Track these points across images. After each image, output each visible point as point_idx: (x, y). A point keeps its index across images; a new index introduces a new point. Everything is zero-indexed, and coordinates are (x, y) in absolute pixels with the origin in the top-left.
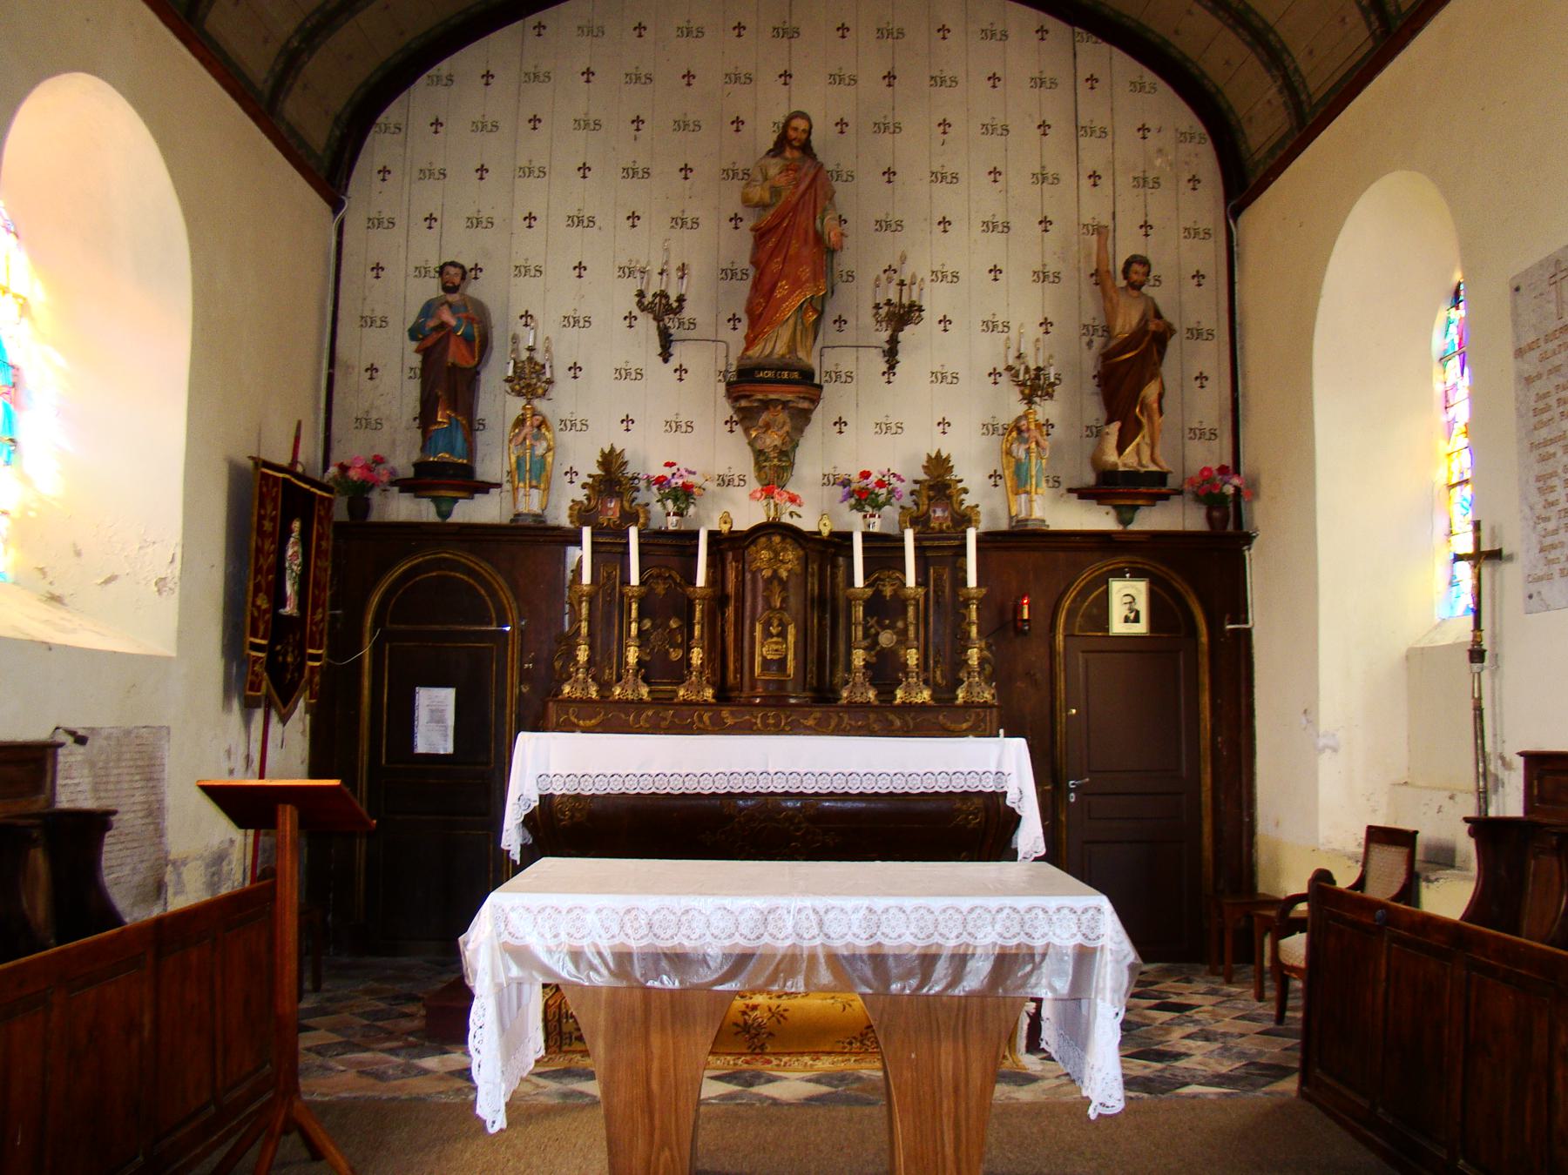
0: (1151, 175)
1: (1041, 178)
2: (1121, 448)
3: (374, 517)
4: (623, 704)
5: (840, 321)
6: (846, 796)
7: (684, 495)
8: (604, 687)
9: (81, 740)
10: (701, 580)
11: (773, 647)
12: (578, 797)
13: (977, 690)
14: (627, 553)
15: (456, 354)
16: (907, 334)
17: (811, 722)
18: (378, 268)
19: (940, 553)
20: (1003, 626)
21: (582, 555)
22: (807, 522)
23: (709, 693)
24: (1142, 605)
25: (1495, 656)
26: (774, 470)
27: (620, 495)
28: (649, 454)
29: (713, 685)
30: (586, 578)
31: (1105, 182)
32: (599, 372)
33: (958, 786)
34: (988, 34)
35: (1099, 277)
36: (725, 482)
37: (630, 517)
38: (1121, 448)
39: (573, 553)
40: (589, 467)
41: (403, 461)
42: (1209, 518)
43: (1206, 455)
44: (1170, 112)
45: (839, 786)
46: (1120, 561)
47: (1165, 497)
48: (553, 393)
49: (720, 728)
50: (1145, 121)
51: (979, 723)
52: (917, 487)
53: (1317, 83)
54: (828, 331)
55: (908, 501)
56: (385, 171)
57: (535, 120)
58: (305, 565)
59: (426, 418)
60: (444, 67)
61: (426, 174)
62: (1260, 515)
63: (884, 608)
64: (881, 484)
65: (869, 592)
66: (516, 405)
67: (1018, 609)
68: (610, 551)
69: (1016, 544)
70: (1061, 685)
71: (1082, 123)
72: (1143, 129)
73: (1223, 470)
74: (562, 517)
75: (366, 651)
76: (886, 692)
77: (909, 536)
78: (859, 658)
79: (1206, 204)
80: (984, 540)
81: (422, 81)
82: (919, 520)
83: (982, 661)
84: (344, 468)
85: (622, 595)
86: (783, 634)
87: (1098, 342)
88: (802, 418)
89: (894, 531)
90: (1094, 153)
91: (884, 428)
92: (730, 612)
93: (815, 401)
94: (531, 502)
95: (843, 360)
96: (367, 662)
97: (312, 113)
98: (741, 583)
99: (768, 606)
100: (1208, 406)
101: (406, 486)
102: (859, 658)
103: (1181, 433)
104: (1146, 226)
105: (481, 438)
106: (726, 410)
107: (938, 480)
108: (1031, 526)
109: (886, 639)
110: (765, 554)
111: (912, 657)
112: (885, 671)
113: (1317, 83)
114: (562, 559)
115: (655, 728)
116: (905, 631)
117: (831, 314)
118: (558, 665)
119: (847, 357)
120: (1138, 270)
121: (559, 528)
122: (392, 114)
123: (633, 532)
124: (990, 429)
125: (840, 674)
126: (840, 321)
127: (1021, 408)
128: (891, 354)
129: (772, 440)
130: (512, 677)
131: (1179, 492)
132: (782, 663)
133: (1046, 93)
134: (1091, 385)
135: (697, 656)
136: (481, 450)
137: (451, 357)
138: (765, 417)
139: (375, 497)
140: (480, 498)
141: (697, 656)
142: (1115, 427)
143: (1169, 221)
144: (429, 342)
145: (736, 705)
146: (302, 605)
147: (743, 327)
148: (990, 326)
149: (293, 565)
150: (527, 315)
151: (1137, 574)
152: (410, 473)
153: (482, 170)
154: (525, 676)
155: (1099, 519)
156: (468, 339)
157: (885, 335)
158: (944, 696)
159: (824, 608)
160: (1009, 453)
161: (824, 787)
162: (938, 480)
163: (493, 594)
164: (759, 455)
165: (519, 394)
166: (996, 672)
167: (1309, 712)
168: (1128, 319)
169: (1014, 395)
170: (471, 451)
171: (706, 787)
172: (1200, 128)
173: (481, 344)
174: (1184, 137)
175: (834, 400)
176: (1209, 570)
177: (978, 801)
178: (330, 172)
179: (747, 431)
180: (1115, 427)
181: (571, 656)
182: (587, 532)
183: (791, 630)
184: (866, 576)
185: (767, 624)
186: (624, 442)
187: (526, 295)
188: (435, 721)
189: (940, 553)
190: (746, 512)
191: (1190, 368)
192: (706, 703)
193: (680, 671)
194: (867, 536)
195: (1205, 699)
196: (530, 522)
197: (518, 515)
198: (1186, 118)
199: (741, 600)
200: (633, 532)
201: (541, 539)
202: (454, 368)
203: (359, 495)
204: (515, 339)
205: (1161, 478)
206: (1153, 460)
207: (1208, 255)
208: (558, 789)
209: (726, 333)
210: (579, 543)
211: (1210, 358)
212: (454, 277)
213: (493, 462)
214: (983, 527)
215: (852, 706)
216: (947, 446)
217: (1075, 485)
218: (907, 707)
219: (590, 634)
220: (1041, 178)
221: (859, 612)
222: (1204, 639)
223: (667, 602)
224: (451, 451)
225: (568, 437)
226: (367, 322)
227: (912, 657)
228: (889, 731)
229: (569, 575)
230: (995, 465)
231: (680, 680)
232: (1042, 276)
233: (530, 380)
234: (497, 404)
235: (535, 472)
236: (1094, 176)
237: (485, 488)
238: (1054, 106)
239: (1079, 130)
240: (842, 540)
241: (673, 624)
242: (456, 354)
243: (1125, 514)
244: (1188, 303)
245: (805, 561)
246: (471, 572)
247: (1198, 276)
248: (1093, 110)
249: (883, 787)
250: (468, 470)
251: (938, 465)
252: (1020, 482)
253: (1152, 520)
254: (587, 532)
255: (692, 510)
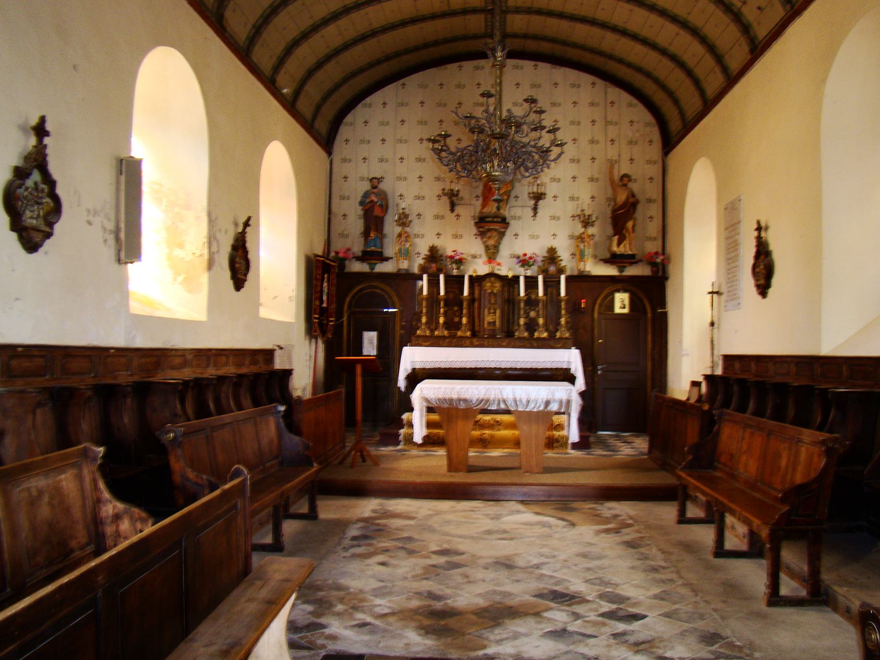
0: (634, 140)
1: (592, 142)
2: (619, 244)
3: (347, 270)
4: (438, 337)
5: (516, 197)
6: (516, 369)
7: (460, 262)
8: (432, 331)
9: (281, 348)
10: (466, 293)
11: (491, 317)
12: (424, 369)
13: (563, 333)
14: (439, 283)
15: (377, 212)
16: (541, 202)
17: (504, 344)
18: (346, 177)
19: (552, 283)
20: (574, 309)
21: (424, 283)
22: (503, 271)
23: (468, 334)
24: (627, 302)
25: (719, 325)
26: (492, 253)
27: (436, 262)
28: (449, 247)
29: (470, 330)
30: (425, 292)
31: (616, 143)
32: (428, 215)
33: (554, 366)
34: (573, 86)
35: (612, 182)
36: (474, 257)
37: (440, 271)
38: (619, 244)
39: (420, 283)
40: (424, 251)
41: (357, 248)
42: (652, 271)
43: (652, 247)
44: (641, 114)
45: (513, 366)
46: (619, 286)
47: (636, 263)
48: (411, 225)
49: (472, 345)
50: (633, 117)
51: (564, 344)
52: (435, 417)
53: (761, 32)
54: (512, 201)
55: (540, 264)
56: (347, 140)
57: (403, 121)
58: (328, 289)
59: (366, 234)
60: (368, 100)
61: (362, 142)
62: (672, 269)
63: (531, 302)
64: (531, 258)
65: (525, 298)
66: (398, 229)
67: (580, 304)
68: (434, 283)
69: (578, 280)
70: (596, 331)
71: (609, 119)
72: (631, 122)
73: (656, 253)
74: (416, 270)
75: (345, 318)
76: (531, 334)
77: (540, 279)
78: (522, 321)
79: (655, 151)
80: (569, 279)
81: (360, 105)
82: (544, 271)
83: (567, 322)
84: (337, 253)
85: (437, 298)
86: (495, 313)
87: (612, 204)
88: (502, 234)
89: (535, 274)
90: (612, 132)
91: (533, 237)
92: (476, 304)
93: (506, 228)
94: (404, 265)
95: (517, 211)
96: (345, 323)
97: (322, 125)
98: (480, 294)
99: (490, 303)
100: (653, 228)
101: (358, 259)
102: (522, 321)
103: (642, 238)
104: (631, 160)
105: (386, 241)
106: (474, 230)
107: (552, 256)
108: (586, 274)
109: (532, 314)
110: (489, 284)
111: (541, 321)
112: (531, 326)
113: (690, 113)
114: (415, 285)
115: (450, 345)
116: (538, 311)
117: (513, 194)
118: (414, 323)
119: (518, 211)
120: (626, 178)
121: (413, 274)
122: (349, 118)
123: (442, 277)
124: (572, 237)
125: (516, 327)
126: (516, 197)
127: (583, 230)
128: (535, 209)
129: (491, 242)
130: (398, 327)
131: (641, 261)
132: (494, 323)
133: (594, 108)
134: (609, 221)
135: (464, 320)
136: (385, 247)
137: (374, 211)
138: (489, 234)
139: (347, 262)
140: (385, 263)
141: (464, 320)
142: (616, 237)
143: (639, 159)
144: (367, 207)
145: (479, 337)
146: (328, 304)
147: (481, 199)
148: (572, 199)
149: (326, 290)
150: (401, 195)
151: (625, 291)
152: (360, 254)
153: (383, 140)
154: (402, 327)
155: (610, 271)
156: (381, 206)
157: (533, 202)
158: (552, 336)
159: (510, 302)
160: (578, 246)
161: (508, 366)
162: (552, 256)
163: (391, 297)
164: (487, 248)
165: (400, 225)
166: (573, 327)
167: (681, 342)
168: (622, 197)
169: (580, 225)
170: (382, 247)
171: (468, 366)
172: (653, 121)
173: (385, 208)
174: (647, 125)
175: (514, 226)
176: (653, 291)
177: (561, 372)
178: (327, 142)
179: (482, 238)
180: (616, 237)
181: (419, 320)
182: (425, 277)
183: (498, 312)
184: (526, 290)
185: (490, 309)
186: (438, 243)
187: (401, 188)
188: (370, 343)
189: (552, 283)
190: (481, 268)
191: (648, 213)
192: (467, 337)
193: (458, 326)
194: (526, 277)
195: (649, 337)
196: (403, 272)
197: (400, 270)
198: (648, 117)
199: (480, 299)
200: (442, 277)
201: (408, 278)
202: (377, 217)
203: (341, 262)
204: (397, 205)
205: (633, 256)
206: (631, 250)
207: (655, 171)
208: (418, 366)
209: (474, 201)
210: (422, 279)
211: (655, 210)
212: (375, 182)
213: (390, 250)
214: (568, 273)
215: (520, 338)
216: (555, 243)
217: (602, 257)
218: (539, 339)
219: (427, 312)
220: (592, 142)
221: (522, 305)
222: (649, 315)
223: (454, 300)
224: (375, 246)
225: (417, 240)
226: (343, 198)
227: (541, 321)
228: (532, 347)
229: (417, 291)
230: (572, 251)
231: (459, 329)
232: (592, 179)
233: (404, 220)
234: (391, 228)
235: (406, 254)
236: (612, 140)
237: (387, 259)
238: (597, 114)
239: (607, 123)
240: (516, 278)
241: (456, 308)
242: (377, 212)
243: (621, 269)
244: (645, 188)
245: (503, 286)
246: (382, 290)
247: (651, 178)
248: (612, 115)
249: (528, 366)
250: (381, 253)
251: (552, 251)
252: (582, 257)
253: (632, 271)
254: (425, 277)
255: (462, 267)
